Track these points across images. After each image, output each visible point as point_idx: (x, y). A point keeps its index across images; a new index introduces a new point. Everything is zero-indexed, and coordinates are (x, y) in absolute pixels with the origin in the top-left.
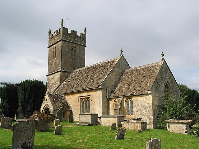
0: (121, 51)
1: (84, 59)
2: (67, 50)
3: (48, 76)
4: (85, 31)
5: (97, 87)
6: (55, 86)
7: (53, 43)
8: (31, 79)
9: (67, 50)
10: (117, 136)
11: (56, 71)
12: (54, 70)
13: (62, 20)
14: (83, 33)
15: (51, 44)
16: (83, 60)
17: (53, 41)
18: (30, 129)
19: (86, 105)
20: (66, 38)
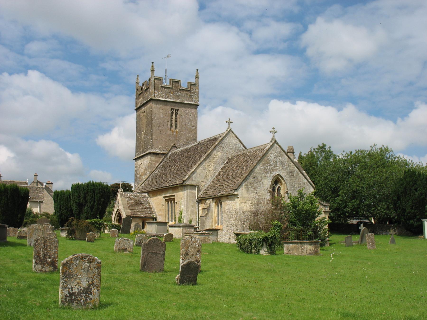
0: (229, 122)
1: (194, 128)
2: (162, 116)
3: (136, 159)
4: (197, 77)
5: (181, 184)
6: (143, 176)
7: (141, 103)
8: (323, 107)
9: (162, 116)
10: (136, 242)
11: (145, 152)
12: (143, 150)
13: (153, 63)
14: (193, 81)
15: (139, 105)
16: (193, 130)
17: (141, 101)
18: (40, 229)
19: (172, 210)
20: (159, 95)
